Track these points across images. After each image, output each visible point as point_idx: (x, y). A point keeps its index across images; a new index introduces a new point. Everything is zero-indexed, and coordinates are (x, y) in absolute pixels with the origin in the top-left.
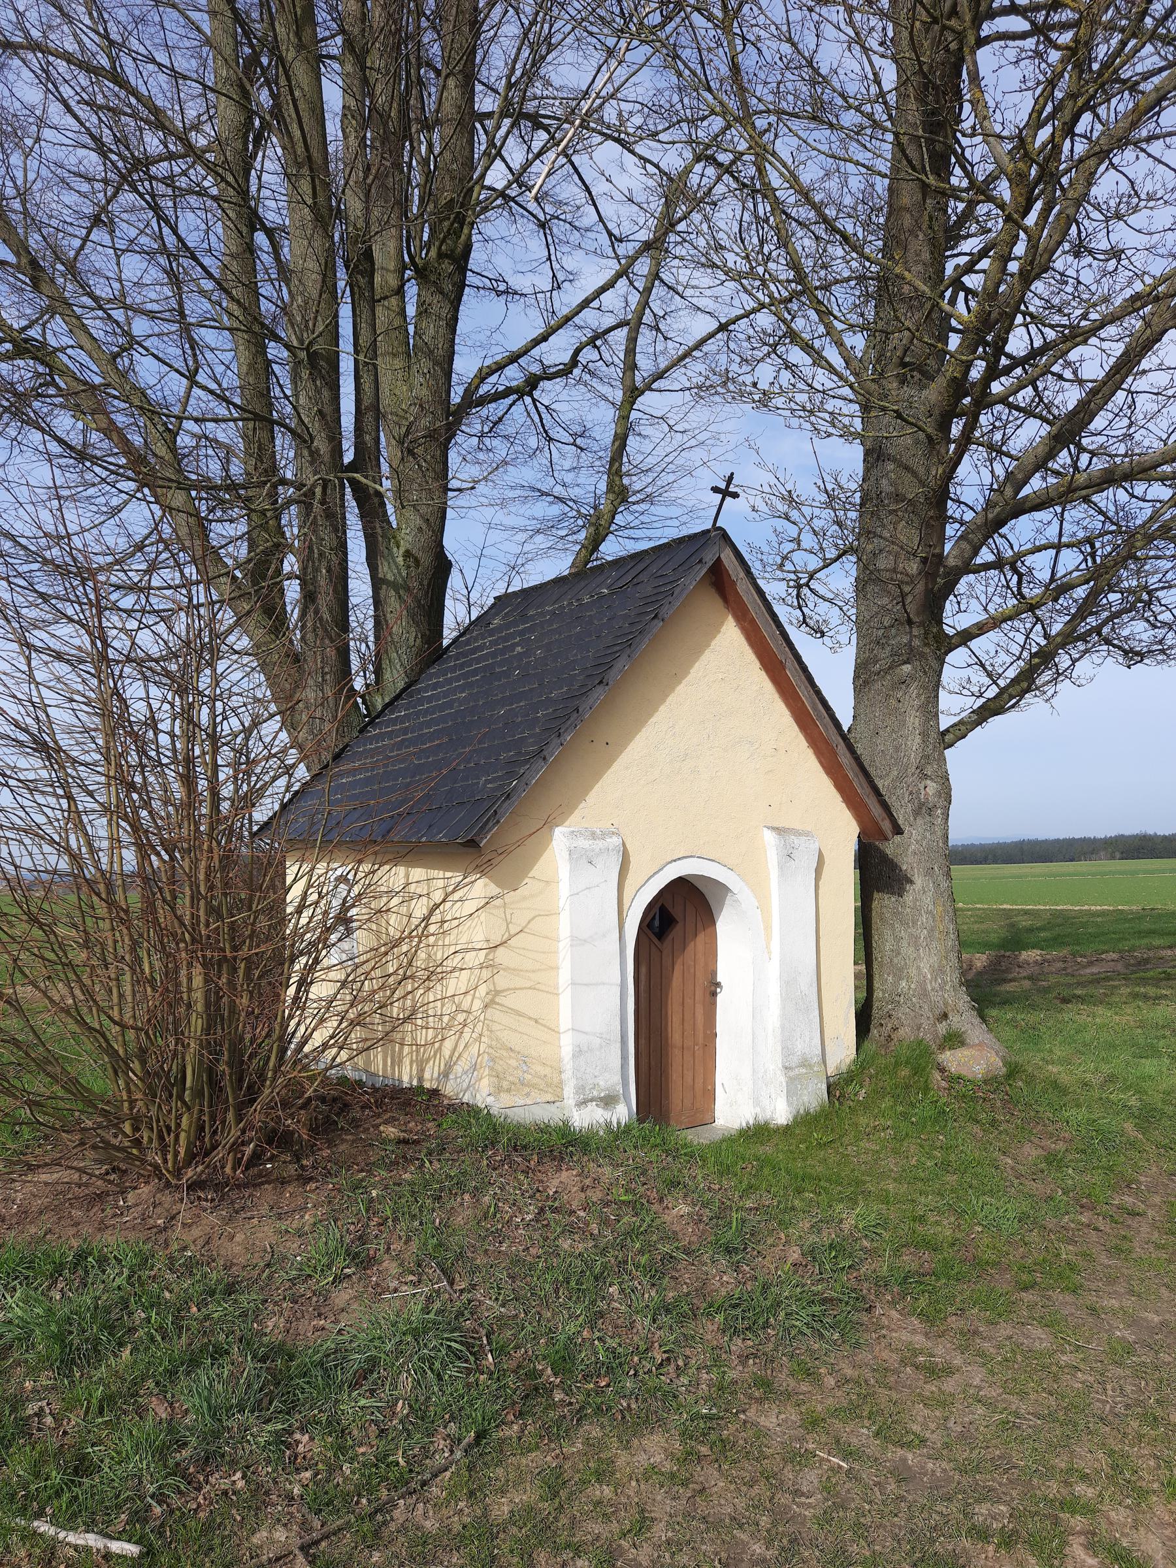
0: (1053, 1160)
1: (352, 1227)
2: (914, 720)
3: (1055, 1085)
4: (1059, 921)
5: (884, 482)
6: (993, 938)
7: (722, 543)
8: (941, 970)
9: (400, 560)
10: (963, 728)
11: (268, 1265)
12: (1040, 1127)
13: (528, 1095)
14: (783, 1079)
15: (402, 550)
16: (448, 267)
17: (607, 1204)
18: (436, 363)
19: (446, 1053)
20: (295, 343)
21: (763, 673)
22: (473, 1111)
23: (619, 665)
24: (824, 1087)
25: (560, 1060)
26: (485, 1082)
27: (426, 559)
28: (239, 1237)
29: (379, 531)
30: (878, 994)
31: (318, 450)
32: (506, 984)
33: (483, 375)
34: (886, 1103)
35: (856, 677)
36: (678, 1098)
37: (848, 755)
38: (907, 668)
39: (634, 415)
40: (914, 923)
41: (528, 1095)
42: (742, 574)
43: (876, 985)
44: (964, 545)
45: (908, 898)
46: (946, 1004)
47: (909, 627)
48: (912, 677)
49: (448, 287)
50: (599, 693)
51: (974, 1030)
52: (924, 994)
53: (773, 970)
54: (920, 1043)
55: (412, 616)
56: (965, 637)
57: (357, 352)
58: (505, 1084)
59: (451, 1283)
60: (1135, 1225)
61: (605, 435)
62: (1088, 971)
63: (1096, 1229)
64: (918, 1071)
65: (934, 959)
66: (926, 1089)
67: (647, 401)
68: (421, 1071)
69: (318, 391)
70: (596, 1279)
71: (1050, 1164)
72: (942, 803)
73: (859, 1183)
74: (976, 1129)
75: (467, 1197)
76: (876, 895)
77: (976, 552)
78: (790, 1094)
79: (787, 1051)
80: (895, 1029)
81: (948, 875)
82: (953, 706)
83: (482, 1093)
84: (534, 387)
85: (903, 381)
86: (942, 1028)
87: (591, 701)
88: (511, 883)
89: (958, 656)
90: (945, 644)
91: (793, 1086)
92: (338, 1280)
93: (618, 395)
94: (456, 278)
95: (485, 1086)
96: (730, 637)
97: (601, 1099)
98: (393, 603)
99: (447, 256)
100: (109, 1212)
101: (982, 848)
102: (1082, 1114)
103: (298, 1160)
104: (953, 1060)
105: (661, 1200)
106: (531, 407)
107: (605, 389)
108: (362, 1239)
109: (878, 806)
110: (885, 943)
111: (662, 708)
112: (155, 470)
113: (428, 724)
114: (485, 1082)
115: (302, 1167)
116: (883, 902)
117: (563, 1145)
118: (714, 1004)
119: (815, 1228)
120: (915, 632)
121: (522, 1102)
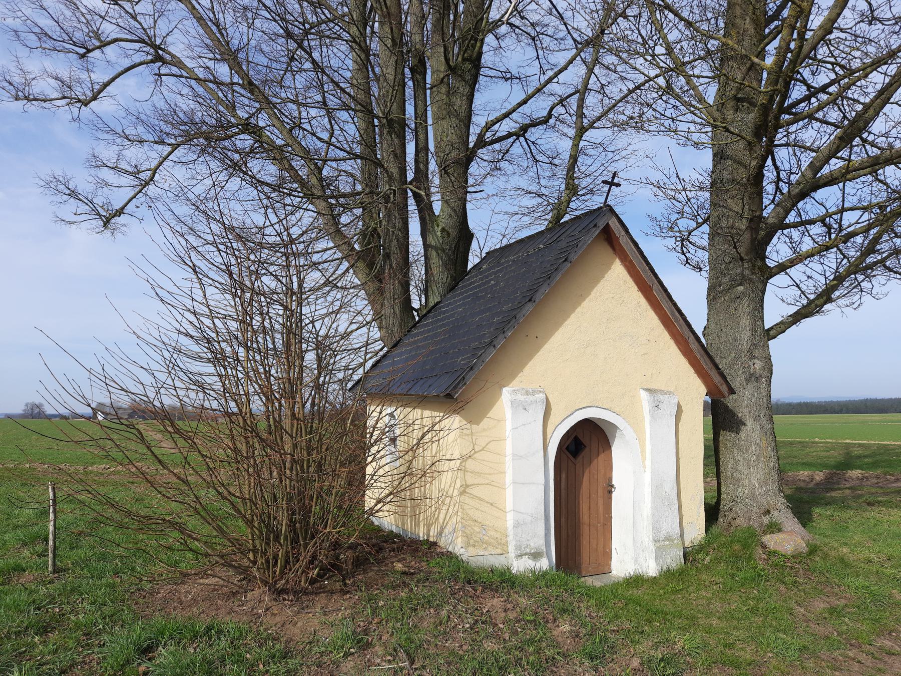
0: (833, 611)
1: (362, 624)
2: (745, 321)
3: (842, 560)
4: (882, 451)
5: (725, 173)
6: (832, 462)
7: (610, 214)
8: (765, 482)
9: (439, 234)
10: (782, 326)
11: (310, 643)
12: (828, 589)
13: (486, 549)
14: (653, 548)
15: (440, 228)
16: (468, 66)
17: (519, 621)
18: (461, 121)
19: (441, 521)
20: (381, 115)
21: (640, 294)
22: (450, 556)
23: (542, 290)
24: (681, 554)
25: (506, 529)
26: (460, 540)
27: (454, 233)
28: (300, 624)
29: (427, 217)
30: (724, 496)
31: (392, 174)
32: (477, 481)
33: (489, 126)
34: (721, 567)
35: (709, 295)
36: (586, 556)
37: (696, 343)
38: (740, 288)
39: (582, 143)
40: (747, 450)
41: (486, 549)
42: (623, 233)
43: (723, 490)
44: (779, 209)
45: (743, 435)
46: (769, 504)
47: (742, 263)
48: (744, 294)
49: (468, 77)
50: (530, 307)
51: (790, 522)
52: (753, 496)
53: (647, 478)
54: (750, 528)
55: (445, 265)
56: (782, 268)
57: (416, 119)
58: (472, 542)
59: (412, 663)
60: (890, 661)
61: (566, 156)
62: (894, 485)
63: (859, 662)
64: (746, 546)
65: (760, 475)
66: (750, 558)
67: (590, 135)
68: (429, 530)
69: (392, 140)
70: (501, 668)
71: (831, 614)
72: (766, 374)
73: (694, 618)
74: (783, 588)
75: (432, 610)
76: (722, 433)
77: (787, 213)
78: (658, 557)
79: (656, 530)
80: (734, 519)
81: (771, 421)
82: (774, 310)
83: (458, 547)
84: (526, 131)
85: (737, 110)
86: (766, 520)
87: (524, 312)
88: (474, 419)
89: (780, 279)
90: (770, 273)
91: (659, 552)
92: (347, 655)
93: (572, 132)
94: (473, 71)
95: (459, 542)
96: (617, 272)
97: (531, 554)
98: (435, 260)
99: (467, 60)
100: (236, 603)
101: (838, 403)
102: (860, 581)
103: (344, 580)
104: (772, 541)
105: (555, 621)
106: (524, 143)
107: (566, 130)
108: (366, 632)
109: (717, 375)
110: (728, 463)
111: (573, 316)
112: (317, 190)
113: (441, 327)
114: (460, 540)
115: (345, 585)
116: (726, 437)
117: (502, 581)
118: (611, 498)
119: (655, 647)
120: (746, 265)
121: (482, 553)
